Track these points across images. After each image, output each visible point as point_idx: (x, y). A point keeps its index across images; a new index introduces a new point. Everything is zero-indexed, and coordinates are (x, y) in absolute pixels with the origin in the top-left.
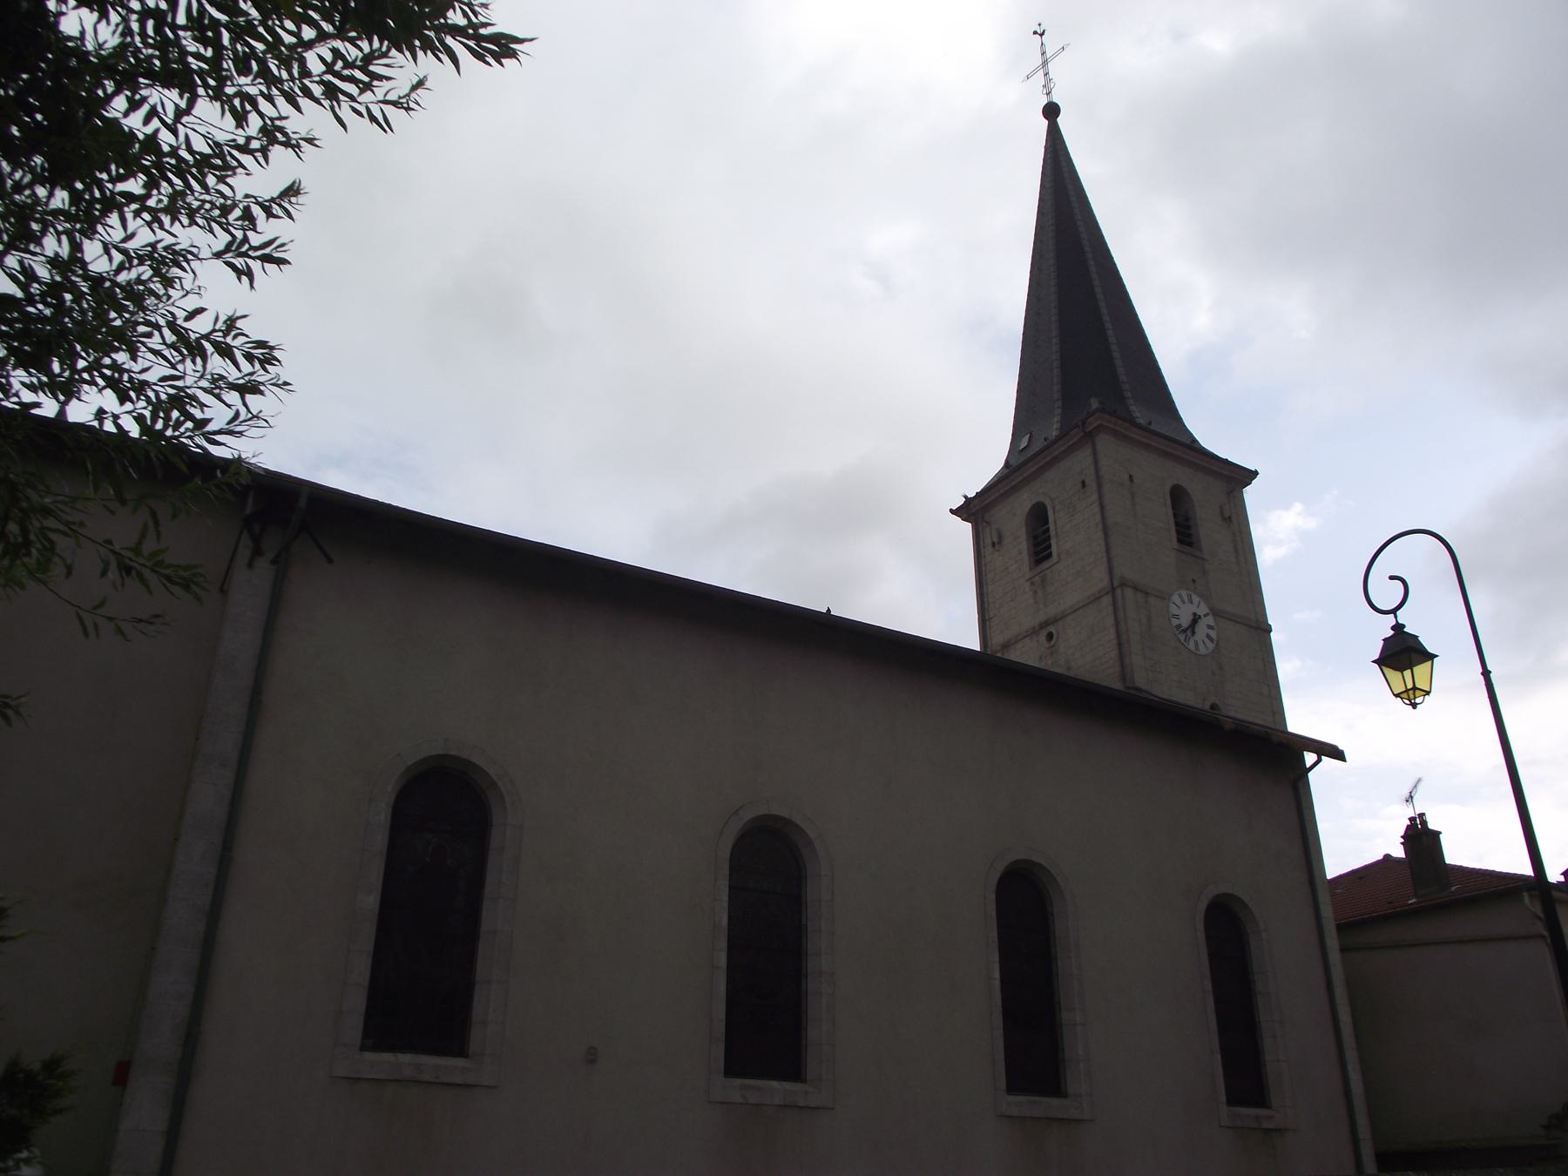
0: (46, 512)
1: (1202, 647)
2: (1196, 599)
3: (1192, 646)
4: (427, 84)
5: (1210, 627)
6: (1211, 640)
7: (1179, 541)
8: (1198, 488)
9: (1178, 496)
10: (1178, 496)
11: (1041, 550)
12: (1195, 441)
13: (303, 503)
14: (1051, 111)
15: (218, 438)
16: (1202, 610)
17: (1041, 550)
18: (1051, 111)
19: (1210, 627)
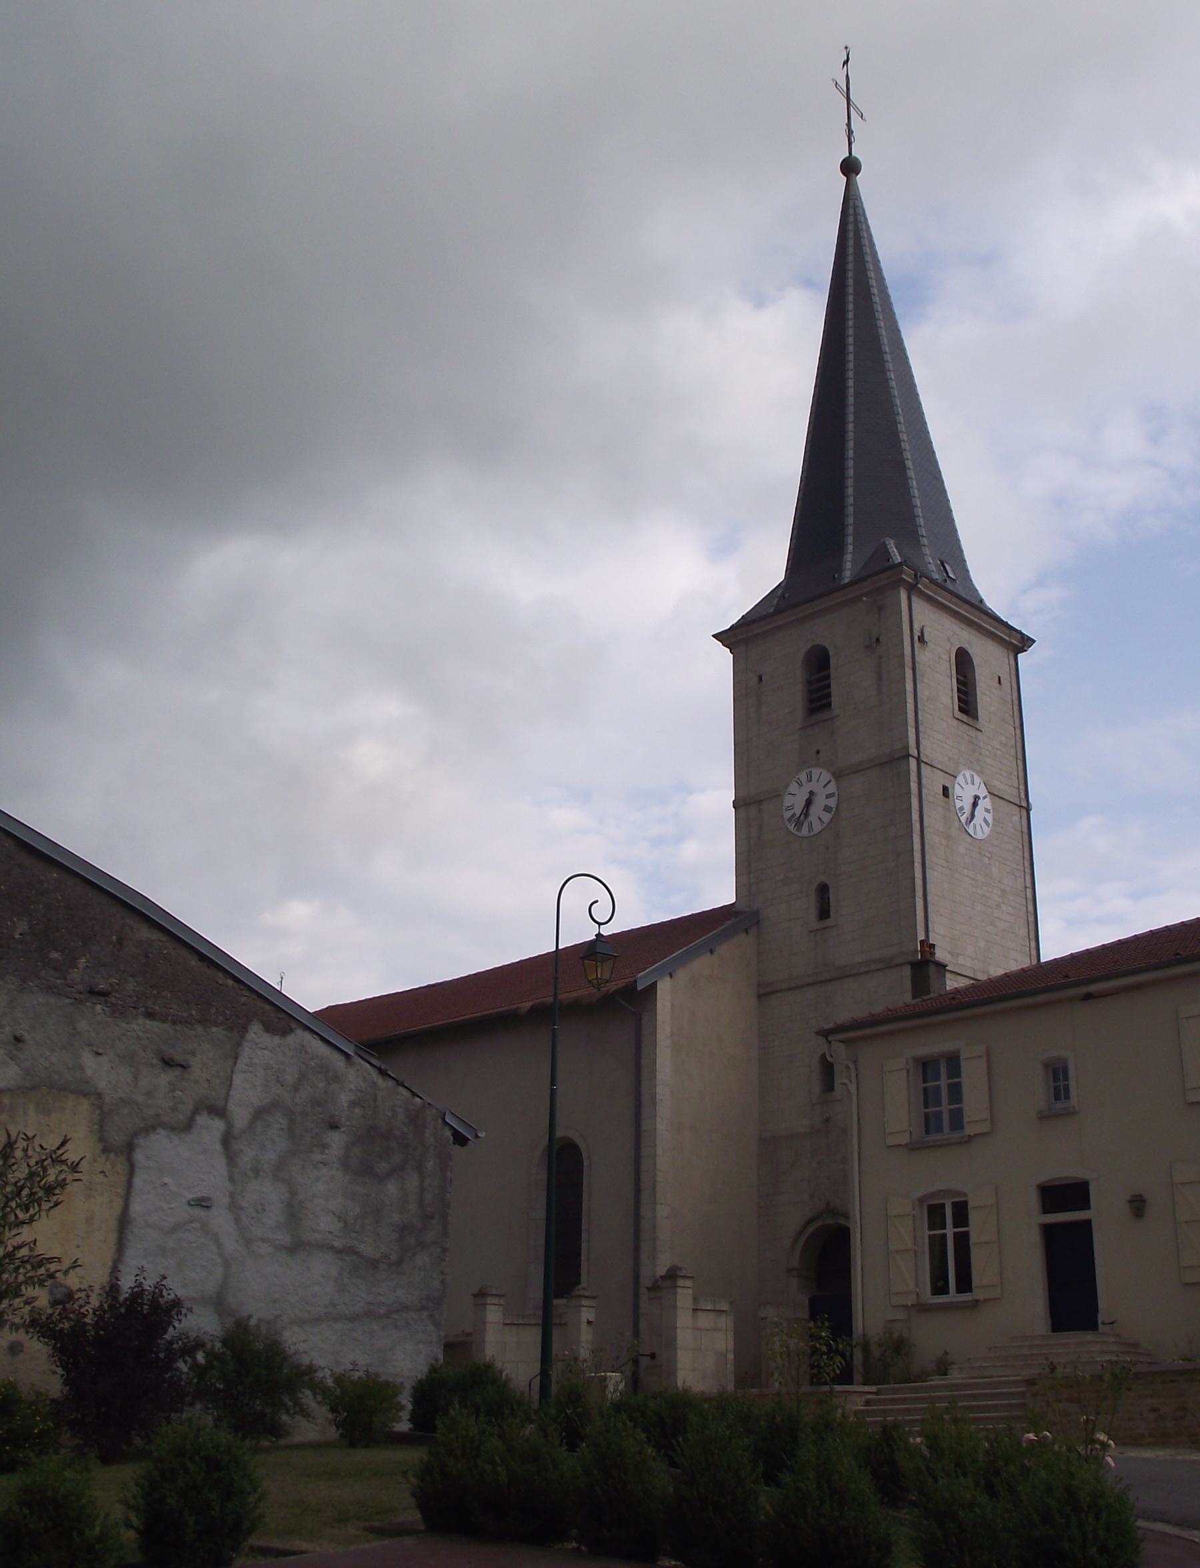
0: (1005, 745)
1: (823, 781)
2: (977, 779)
3: (971, 831)
4: (79, 1263)
5: (987, 810)
6: (988, 824)
7: (961, 709)
8: (986, 656)
9: (963, 661)
10: (963, 661)
11: (818, 699)
12: (981, 601)
13: (406, 1400)
14: (850, 167)
15: (848, 1358)
16: (982, 792)
17: (818, 699)
18: (850, 167)
19: (987, 810)
